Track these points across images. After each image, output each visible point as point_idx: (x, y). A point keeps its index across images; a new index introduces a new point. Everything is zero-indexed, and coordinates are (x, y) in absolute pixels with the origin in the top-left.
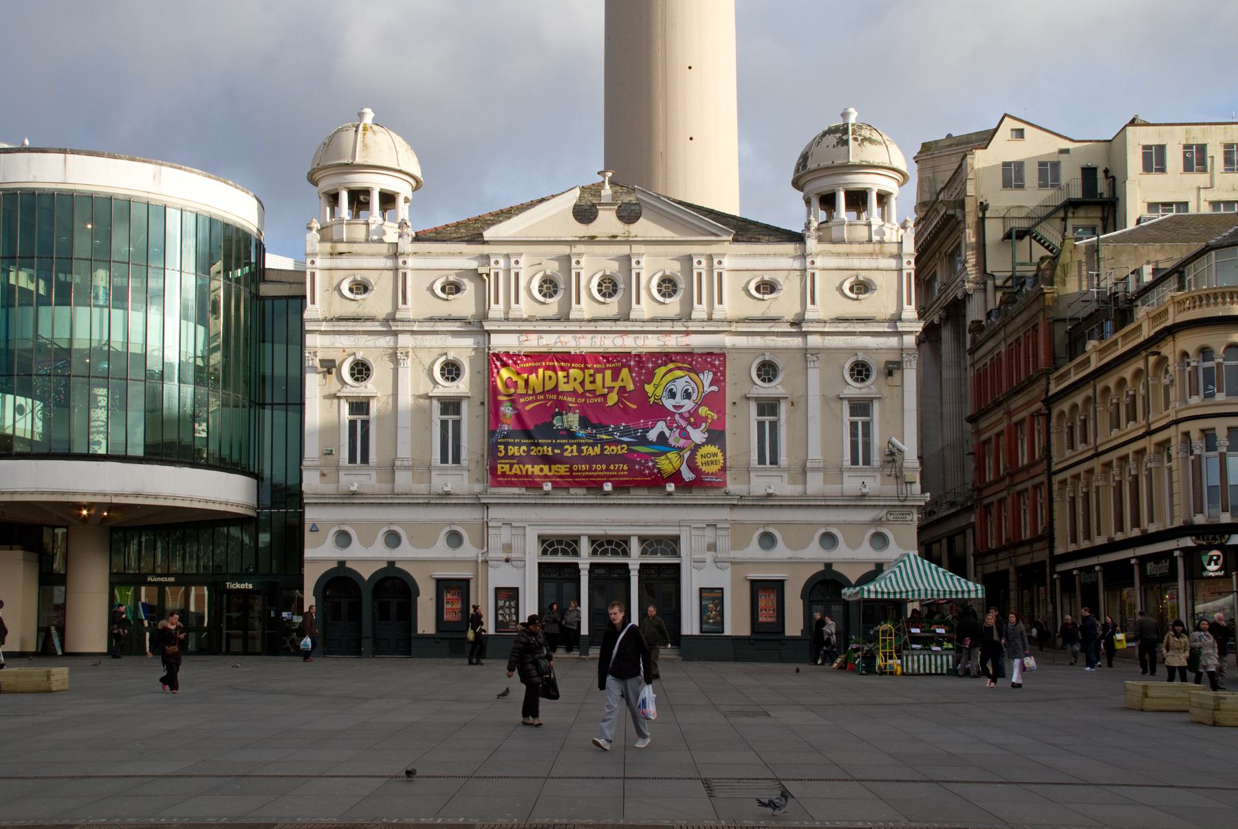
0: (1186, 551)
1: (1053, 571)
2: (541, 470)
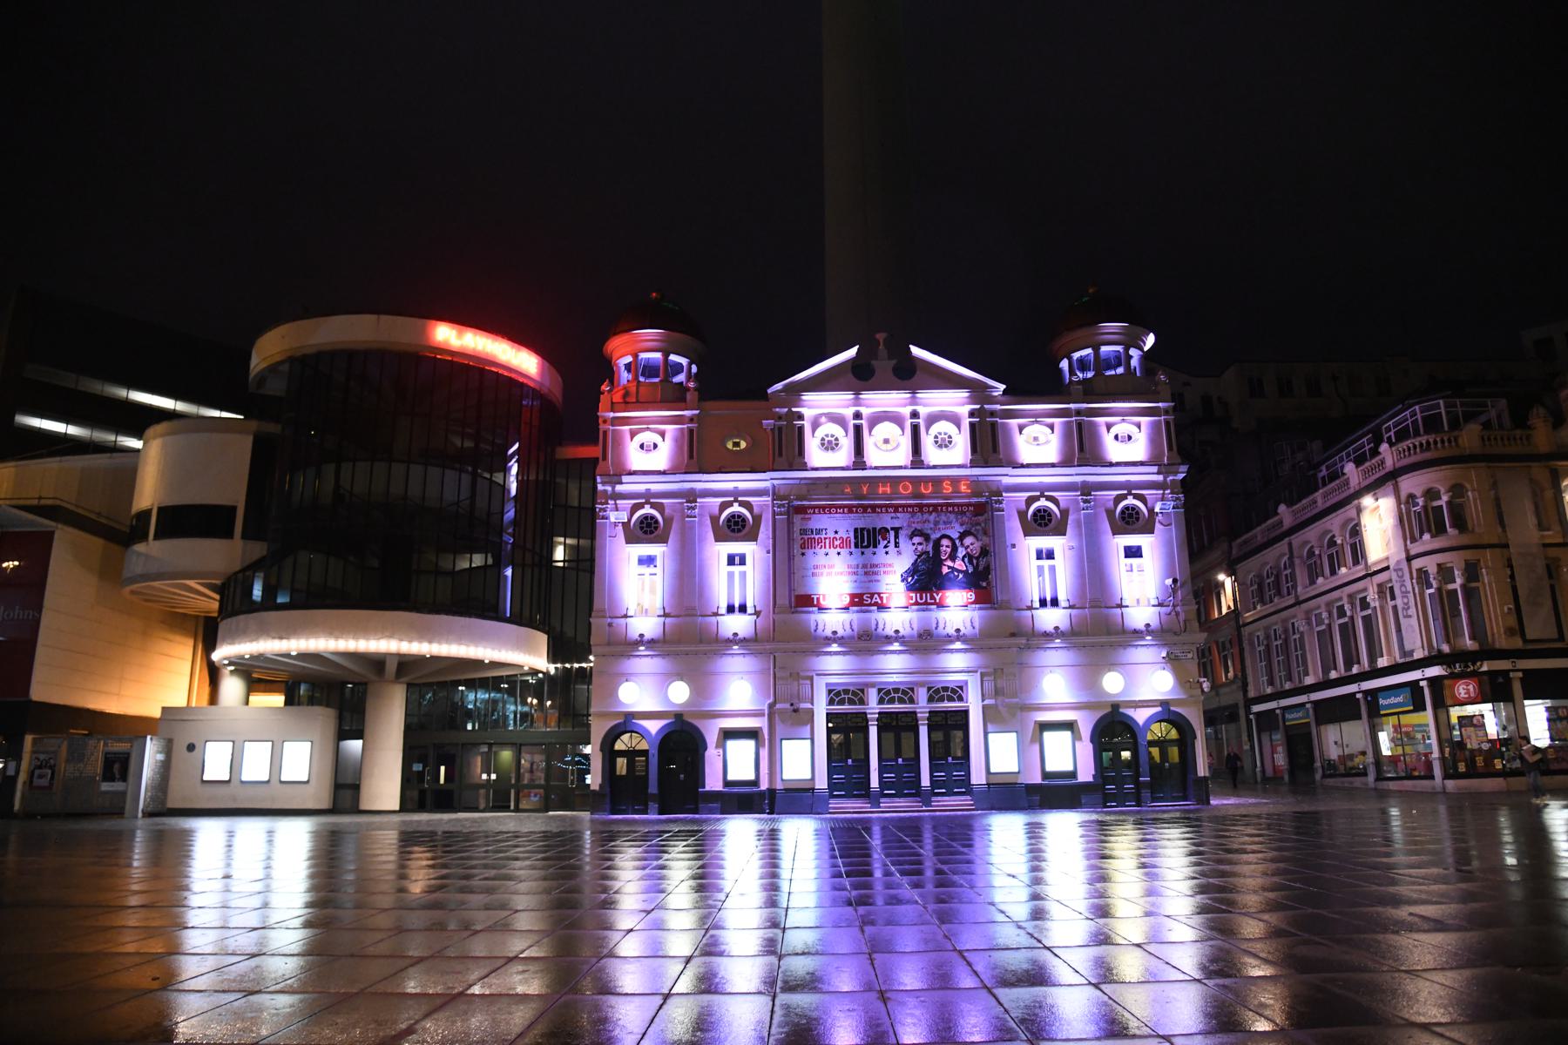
0: (1433, 681)
1: (1248, 711)
2: (737, 444)
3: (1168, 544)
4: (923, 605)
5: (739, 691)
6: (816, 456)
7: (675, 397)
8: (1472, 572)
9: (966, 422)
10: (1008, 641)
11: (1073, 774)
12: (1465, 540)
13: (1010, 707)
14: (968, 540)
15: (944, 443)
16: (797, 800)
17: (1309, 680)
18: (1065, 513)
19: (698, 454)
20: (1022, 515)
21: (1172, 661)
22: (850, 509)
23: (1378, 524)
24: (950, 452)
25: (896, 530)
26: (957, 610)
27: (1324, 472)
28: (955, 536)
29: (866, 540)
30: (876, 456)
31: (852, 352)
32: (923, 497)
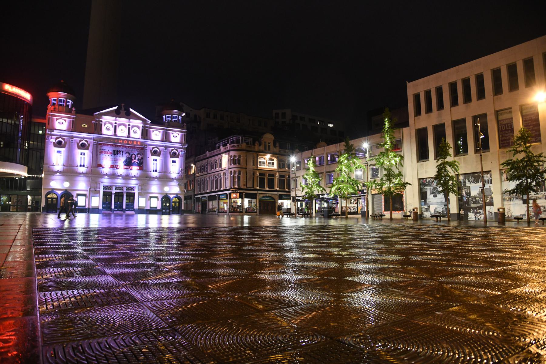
3: (181, 161)
4: (127, 169)
5: (82, 185)
6: (104, 131)
7: (69, 112)
8: (239, 173)
9: (141, 128)
10: (145, 178)
11: (156, 208)
12: (239, 166)
13: (144, 192)
14: (139, 155)
15: (135, 132)
16: (95, 210)
17: (208, 191)
18: (160, 152)
19: (74, 127)
20: (151, 151)
21: (179, 185)
22: (112, 145)
23: (225, 159)
24: (137, 135)
25: (123, 151)
26: (135, 171)
27: (217, 145)
28: (136, 153)
29: (115, 153)
30: (119, 133)
31: (116, 108)
32: (129, 144)
